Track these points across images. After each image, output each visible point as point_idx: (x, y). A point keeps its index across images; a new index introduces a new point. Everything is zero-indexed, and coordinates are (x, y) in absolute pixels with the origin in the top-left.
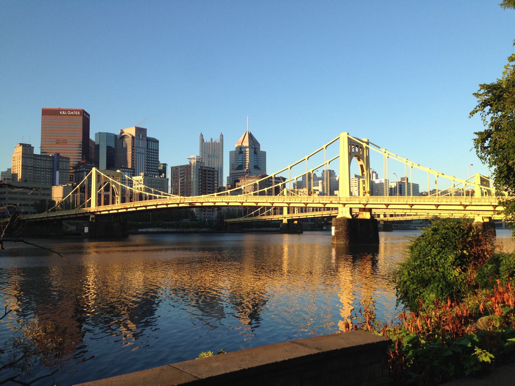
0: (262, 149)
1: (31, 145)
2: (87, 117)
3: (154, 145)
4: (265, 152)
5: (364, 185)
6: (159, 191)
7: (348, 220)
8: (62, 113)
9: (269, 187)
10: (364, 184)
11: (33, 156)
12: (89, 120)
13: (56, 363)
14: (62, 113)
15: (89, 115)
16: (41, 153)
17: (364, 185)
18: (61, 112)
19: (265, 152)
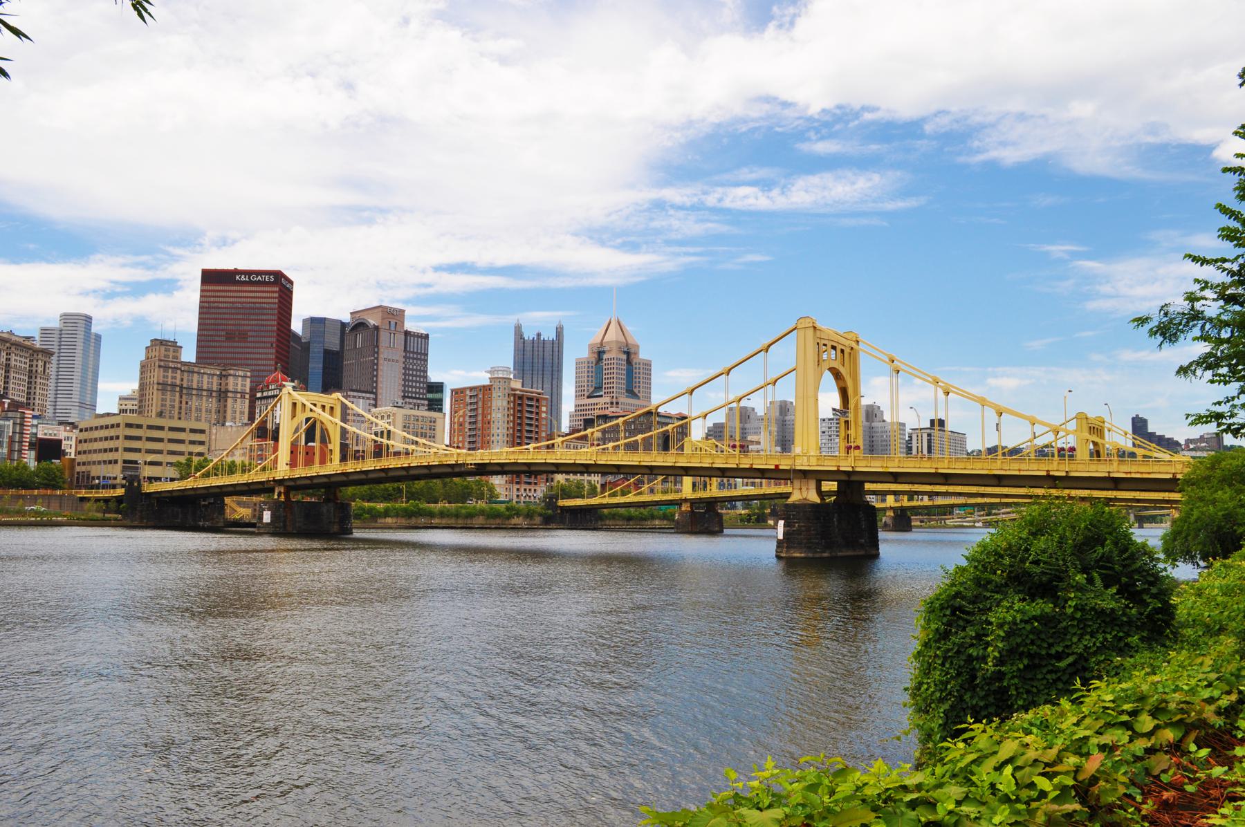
7: (814, 505)
12: (291, 292)
15: (291, 283)
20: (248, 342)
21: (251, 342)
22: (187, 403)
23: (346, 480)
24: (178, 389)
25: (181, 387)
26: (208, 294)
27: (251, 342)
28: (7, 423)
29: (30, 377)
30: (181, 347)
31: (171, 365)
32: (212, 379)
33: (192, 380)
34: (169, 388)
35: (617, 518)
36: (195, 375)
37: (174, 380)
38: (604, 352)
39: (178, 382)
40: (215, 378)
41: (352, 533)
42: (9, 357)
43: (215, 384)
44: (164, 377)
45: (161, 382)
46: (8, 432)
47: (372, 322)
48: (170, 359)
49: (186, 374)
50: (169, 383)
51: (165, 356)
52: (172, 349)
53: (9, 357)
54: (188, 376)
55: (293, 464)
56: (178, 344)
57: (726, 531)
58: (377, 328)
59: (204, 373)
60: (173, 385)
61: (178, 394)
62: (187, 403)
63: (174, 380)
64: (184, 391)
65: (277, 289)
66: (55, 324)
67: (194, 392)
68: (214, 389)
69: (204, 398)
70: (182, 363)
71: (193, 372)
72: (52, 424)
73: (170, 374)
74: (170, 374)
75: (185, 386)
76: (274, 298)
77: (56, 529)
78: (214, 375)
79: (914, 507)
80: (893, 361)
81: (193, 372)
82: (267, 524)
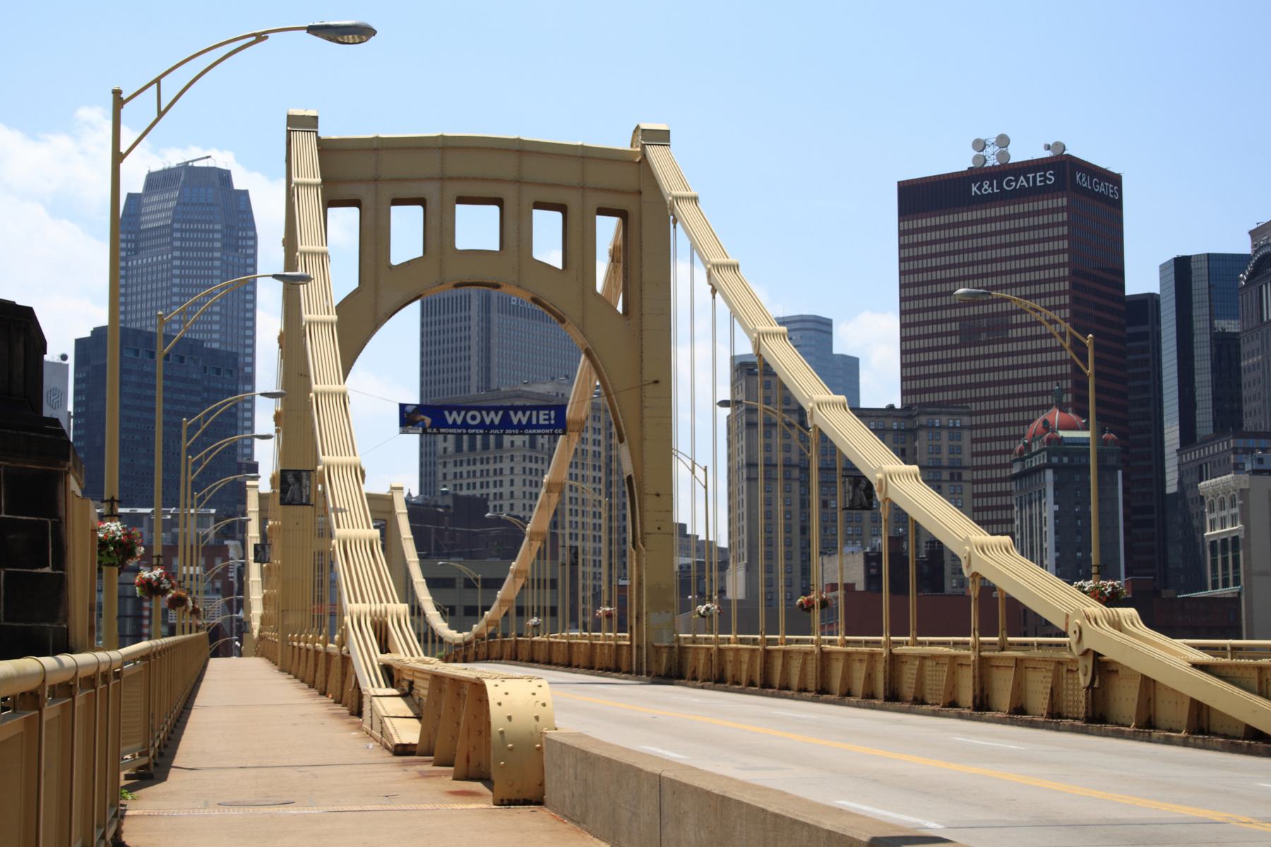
2: (1100, 189)
8: (980, 188)
12: (1117, 205)
14: (980, 188)
16: (904, 393)
21: (1017, 340)
27: (1017, 340)
36: (945, 434)
59: (941, 427)
65: (1063, 202)
76: (1058, 224)
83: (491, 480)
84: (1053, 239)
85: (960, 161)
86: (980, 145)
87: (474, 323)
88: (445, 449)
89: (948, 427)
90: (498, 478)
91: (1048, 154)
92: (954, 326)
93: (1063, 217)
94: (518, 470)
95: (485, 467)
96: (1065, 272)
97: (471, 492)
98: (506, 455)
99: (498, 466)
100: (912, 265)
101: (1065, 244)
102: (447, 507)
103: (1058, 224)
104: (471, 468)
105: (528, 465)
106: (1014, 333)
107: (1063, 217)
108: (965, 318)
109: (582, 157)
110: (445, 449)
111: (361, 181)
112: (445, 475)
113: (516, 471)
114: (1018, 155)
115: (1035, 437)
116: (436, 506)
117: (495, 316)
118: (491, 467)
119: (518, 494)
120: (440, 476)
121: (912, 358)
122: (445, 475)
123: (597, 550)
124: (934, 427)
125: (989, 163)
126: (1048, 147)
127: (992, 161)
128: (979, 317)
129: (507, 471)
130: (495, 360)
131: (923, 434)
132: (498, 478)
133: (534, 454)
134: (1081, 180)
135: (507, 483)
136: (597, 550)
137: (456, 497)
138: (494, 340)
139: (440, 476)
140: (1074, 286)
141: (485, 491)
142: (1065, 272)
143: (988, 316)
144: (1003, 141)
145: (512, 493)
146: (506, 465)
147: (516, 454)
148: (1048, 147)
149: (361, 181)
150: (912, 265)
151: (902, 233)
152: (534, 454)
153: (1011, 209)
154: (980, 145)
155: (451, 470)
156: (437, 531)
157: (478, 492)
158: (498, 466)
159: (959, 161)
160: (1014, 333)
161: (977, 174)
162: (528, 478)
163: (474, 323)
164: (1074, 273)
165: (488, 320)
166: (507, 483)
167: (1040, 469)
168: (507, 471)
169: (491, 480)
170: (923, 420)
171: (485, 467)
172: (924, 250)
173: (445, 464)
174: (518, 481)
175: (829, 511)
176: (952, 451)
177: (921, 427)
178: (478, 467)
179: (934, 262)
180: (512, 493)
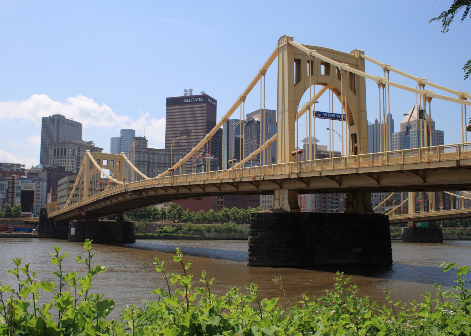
0: (437, 128)
1: (113, 140)
2: (212, 103)
3: (202, 121)
4: (443, 132)
5: (356, 145)
6: (51, 190)
7: (286, 214)
8: (186, 101)
9: (144, 173)
10: (356, 142)
11: (146, 151)
12: (216, 107)
13: (75, 284)
14: (186, 101)
15: (215, 101)
16: (166, 147)
17: (356, 145)
18: (184, 101)
19: (443, 132)
20: (191, 136)
21: (193, 136)
22: (152, 171)
23: (440, 218)
24: (146, 163)
25: (149, 162)
26: (170, 111)
27: (193, 136)
28: (5, 183)
29: (78, 160)
30: (147, 140)
31: (142, 150)
32: (155, 156)
33: (160, 159)
34: (141, 163)
35: (446, 231)
36: (156, 155)
37: (144, 159)
38: (410, 128)
39: (146, 160)
40: (167, 156)
41: (135, 242)
42: (79, 152)
43: (167, 160)
44: (139, 157)
45: (137, 160)
46: (6, 187)
47: (256, 119)
48: (142, 147)
49: (151, 155)
50: (141, 160)
51: (139, 146)
52: (142, 141)
53: (79, 152)
54: (164, 157)
55: (417, 210)
56: (146, 139)
57: (444, 241)
58: (258, 122)
59: (161, 154)
60: (144, 161)
61: (146, 166)
62: (152, 171)
63: (144, 159)
64: (151, 165)
65: (205, 105)
66: (118, 135)
67: (156, 165)
68: (167, 163)
69: (162, 168)
70: (148, 149)
71: (155, 154)
72: (29, 182)
73: (142, 156)
74: (142, 156)
75: (151, 162)
76: (204, 110)
77: (205, 241)
78: (167, 154)
79: (450, 218)
80: (423, 85)
81: (155, 154)
82: (73, 235)
83: (63, 163)
84: (202, 113)
85: (181, 94)
86: (186, 91)
87: (55, 125)
88: (51, 155)
89: (181, 155)
90: (64, 162)
91: (201, 94)
92: (179, 132)
93: (205, 108)
94: (70, 161)
95: (61, 160)
96: (205, 121)
97: (61, 165)
98: (67, 157)
99: (65, 159)
100: (169, 117)
101: (205, 115)
102: (56, 168)
103: (204, 110)
104: (58, 160)
105: (72, 160)
106: (192, 134)
107: (205, 108)
108: (181, 130)
109: (345, 55)
110: (51, 155)
111: (301, 55)
112: (51, 161)
113: (69, 161)
114: (194, 94)
115: (199, 158)
116: (53, 168)
117: (61, 124)
118: (63, 160)
119: (70, 166)
120: (49, 161)
121: (168, 139)
122: (51, 161)
123: (426, 209)
124: (178, 154)
125: (187, 95)
126: (201, 93)
127: (188, 95)
128: (184, 130)
129: (67, 161)
130: (60, 134)
131: (156, 155)
132: (64, 162)
133: (73, 157)
134: (209, 100)
135: (67, 164)
136: (426, 209)
137: (58, 166)
138: (60, 130)
139: (49, 161)
140: (207, 124)
141: (64, 165)
142: (205, 121)
143: (186, 130)
144: (191, 90)
145: (68, 166)
146: (67, 159)
147: (70, 157)
148: (201, 93)
149: (301, 55)
150: (169, 117)
151: (167, 110)
152: (73, 157)
153: (193, 106)
154: (186, 91)
155: (52, 160)
156: (53, 174)
157: (63, 165)
158: (65, 159)
159: (180, 94)
160: (192, 134)
161: (185, 97)
162: (72, 163)
163: (55, 125)
164: (207, 121)
165: (59, 125)
166: (67, 164)
167: (201, 165)
168: (67, 161)
169: (63, 163)
170: (176, 153)
171: (61, 160)
172: (172, 114)
173: (51, 159)
174: (70, 163)
175: (153, 173)
176: (164, 160)
177: (175, 154)
178: (60, 160)
179: (174, 117)
180: (68, 166)
